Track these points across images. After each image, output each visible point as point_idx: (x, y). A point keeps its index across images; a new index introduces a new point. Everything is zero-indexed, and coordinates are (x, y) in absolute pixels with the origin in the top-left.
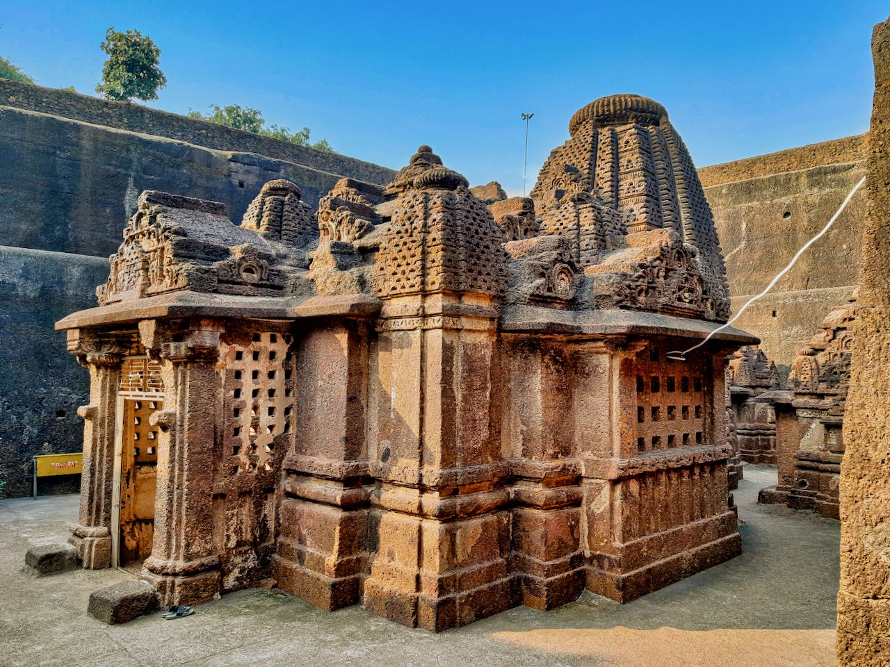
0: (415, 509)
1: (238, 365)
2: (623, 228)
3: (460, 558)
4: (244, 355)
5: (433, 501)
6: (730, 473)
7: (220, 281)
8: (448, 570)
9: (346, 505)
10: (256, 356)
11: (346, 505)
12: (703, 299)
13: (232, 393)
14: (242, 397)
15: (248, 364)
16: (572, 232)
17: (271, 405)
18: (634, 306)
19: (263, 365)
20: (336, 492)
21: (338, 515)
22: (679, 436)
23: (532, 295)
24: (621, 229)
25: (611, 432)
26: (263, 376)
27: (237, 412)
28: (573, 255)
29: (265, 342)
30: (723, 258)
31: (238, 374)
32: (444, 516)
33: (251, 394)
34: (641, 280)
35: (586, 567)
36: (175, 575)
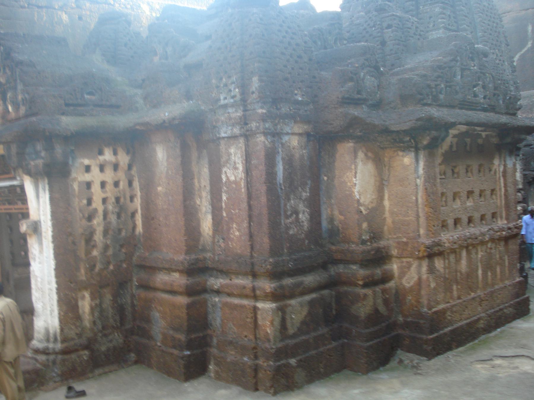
0: (248, 292)
1: (87, 177)
2: (422, 33)
3: (291, 331)
4: (93, 168)
5: (267, 285)
6: (523, 247)
7: (67, 105)
8: (282, 340)
9: (190, 292)
10: (102, 168)
11: (190, 292)
12: (494, 95)
13: (85, 202)
14: (94, 205)
15: (95, 176)
16: (377, 39)
17: (104, 196)
18: (435, 104)
19: (109, 176)
20: (178, 279)
21: (183, 300)
22: (477, 216)
23: (343, 98)
24: (420, 35)
25: (418, 217)
26: (109, 187)
27: (90, 218)
28: (378, 60)
29: (108, 156)
30: (513, 58)
31: (89, 185)
32: (276, 296)
33: (101, 201)
34: (440, 79)
35: (400, 332)
36: (56, 353)
